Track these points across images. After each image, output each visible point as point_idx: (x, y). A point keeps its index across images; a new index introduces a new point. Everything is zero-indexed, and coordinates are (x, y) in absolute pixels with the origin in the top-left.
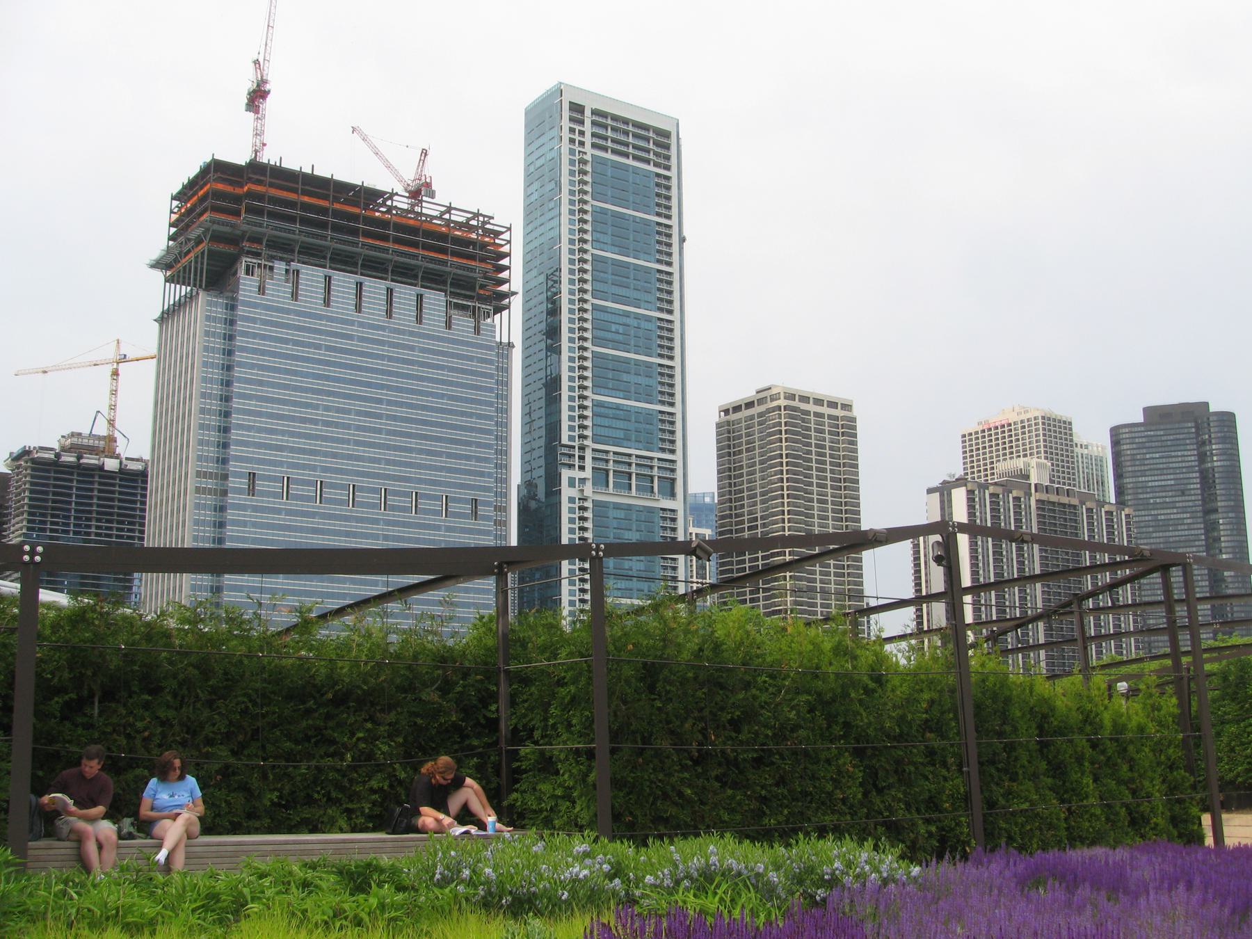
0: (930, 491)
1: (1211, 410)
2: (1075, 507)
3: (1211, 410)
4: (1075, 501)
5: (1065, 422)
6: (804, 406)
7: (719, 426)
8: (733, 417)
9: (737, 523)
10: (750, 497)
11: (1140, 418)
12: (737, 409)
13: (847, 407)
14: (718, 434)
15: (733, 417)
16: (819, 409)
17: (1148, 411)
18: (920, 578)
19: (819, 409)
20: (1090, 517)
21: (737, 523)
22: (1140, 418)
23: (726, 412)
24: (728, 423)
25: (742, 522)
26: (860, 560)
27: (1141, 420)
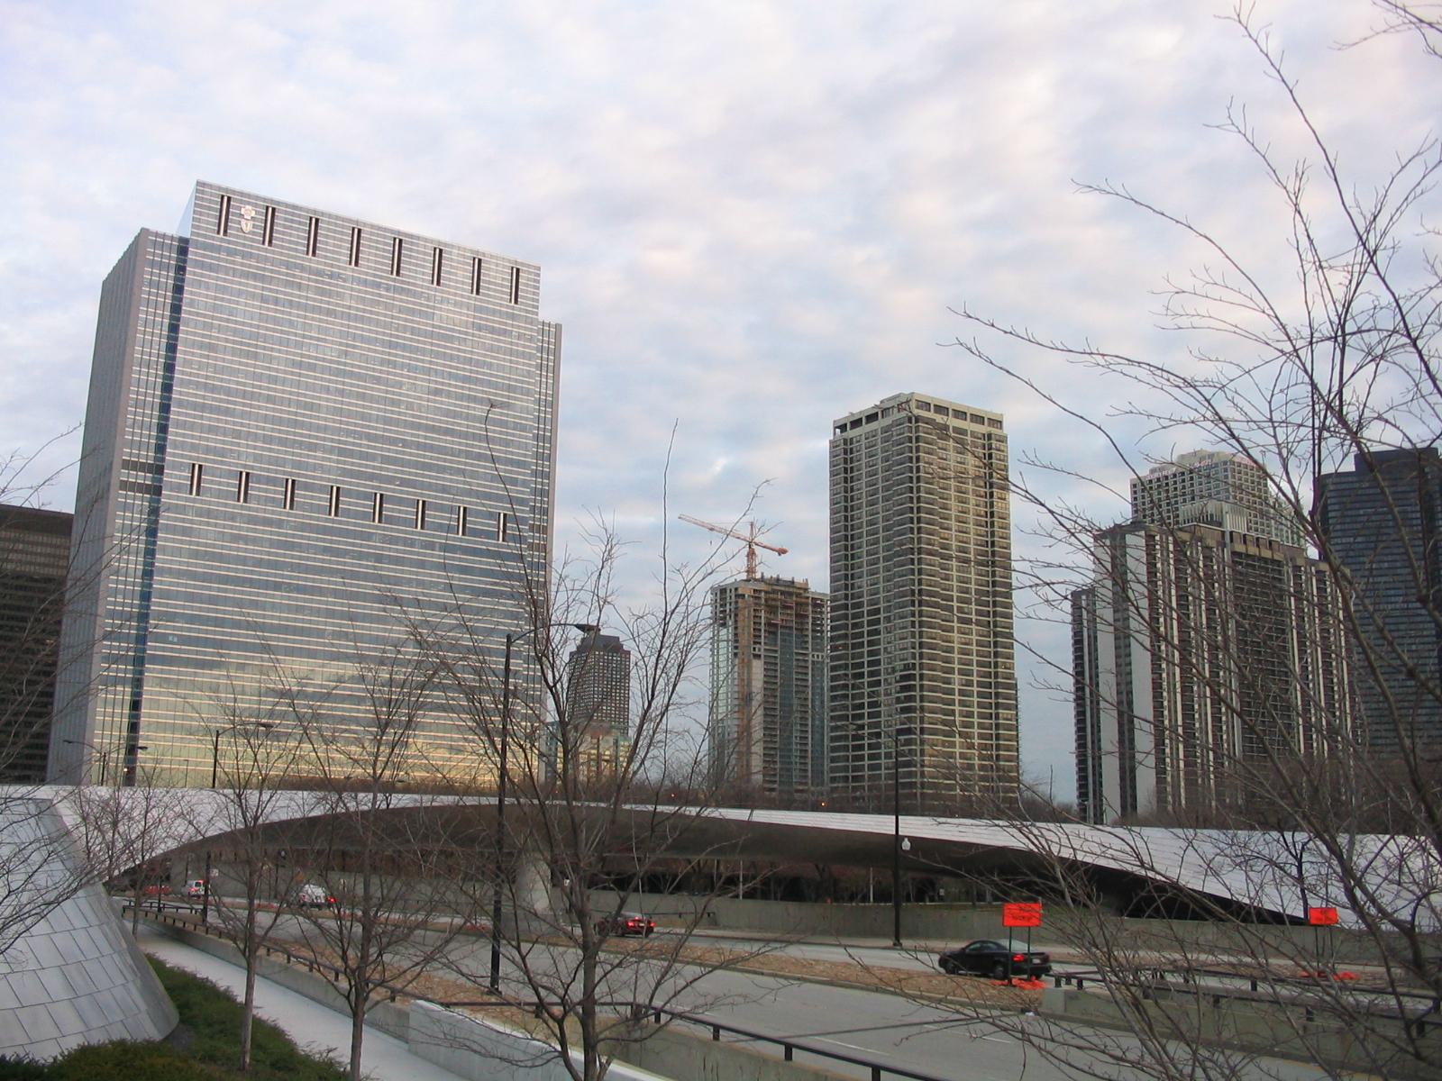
2: (1279, 563)
6: (939, 418)
7: (833, 445)
8: (851, 433)
10: (871, 757)
12: (856, 423)
13: (997, 423)
23: (843, 428)
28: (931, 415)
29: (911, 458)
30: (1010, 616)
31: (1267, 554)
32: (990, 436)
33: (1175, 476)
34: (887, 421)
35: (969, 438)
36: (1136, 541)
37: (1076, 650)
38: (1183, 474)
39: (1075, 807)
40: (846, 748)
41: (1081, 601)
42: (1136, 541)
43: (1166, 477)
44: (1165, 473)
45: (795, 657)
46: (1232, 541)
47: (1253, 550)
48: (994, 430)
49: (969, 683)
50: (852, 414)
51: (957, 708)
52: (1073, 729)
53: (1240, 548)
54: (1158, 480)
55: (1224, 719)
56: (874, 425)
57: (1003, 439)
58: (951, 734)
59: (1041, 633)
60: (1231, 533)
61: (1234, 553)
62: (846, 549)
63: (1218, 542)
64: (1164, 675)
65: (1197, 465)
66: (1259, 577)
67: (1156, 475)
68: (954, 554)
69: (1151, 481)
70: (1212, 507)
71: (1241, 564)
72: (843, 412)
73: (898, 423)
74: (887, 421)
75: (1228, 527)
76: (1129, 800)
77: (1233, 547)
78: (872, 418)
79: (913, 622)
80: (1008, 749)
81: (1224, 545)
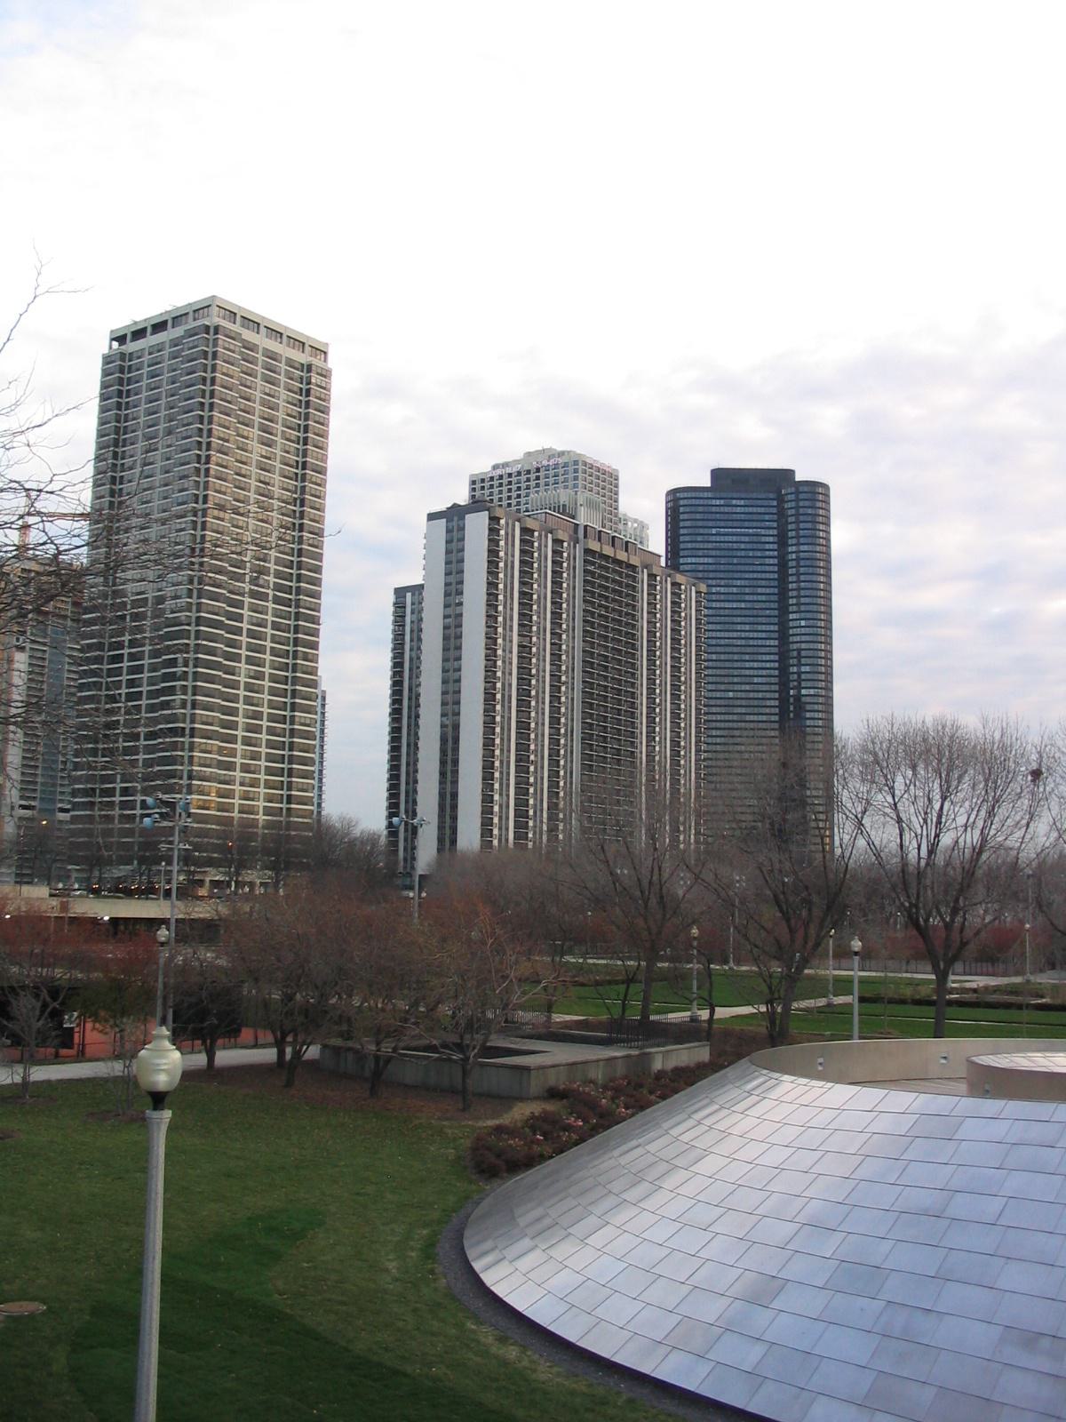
0: (432, 517)
1: (798, 478)
2: (633, 568)
3: (798, 478)
4: (635, 561)
5: (611, 475)
6: (248, 335)
7: (107, 360)
8: (132, 347)
9: (111, 673)
10: (132, 657)
11: (706, 482)
12: (139, 334)
13: (321, 351)
14: (106, 373)
15: (132, 347)
16: (273, 346)
17: (717, 474)
18: (403, 644)
19: (273, 346)
20: (652, 586)
21: (111, 673)
22: (706, 482)
23: (121, 339)
24: (122, 356)
25: (118, 685)
26: (200, 1052)
27: (707, 483)
28: (236, 328)
29: (204, 379)
30: (317, 595)
31: (622, 556)
32: (309, 368)
33: (519, 473)
34: (178, 332)
35: (283, 366)
36: (477, 525)
37: (395, 674)
38: (528, 472)
39: (383, 840)
40: (97, 686)
41: (406, 601)
42: (477, 525)
43: (510, 475)
44: (509, 470)
45: (38, 795)
46: (585, 537)
47: (608, 551)
48: (315, 361)
49: (255, 756)
50: (136, 323)
51: (241, 706)
52: (386, 747)
53: (594, 545)
54: (501, 477)
55: (562, 741)
56: (162, 337)
57: (326, 374)
58: (233, 739)
59: (353, 676)
60: (586, 527)
61: (587, 551)
62: (117, 433)
63: (570, 536)
64: (499, 685)
65: (545, 463)
66: (610, 573)
67: (499, 472)
68: (247, 600)
69: (492, 479)
70: (564, 496)
71: (593, 564)
72: (124, 319)
73: (191, 333)
74: (178, 332)
75: (582, 520)
76: (448, 831)
77: (585, 543)
78: (159, 326)
79: (195, 522)
80: (305, 761)
81: (577, 541)
